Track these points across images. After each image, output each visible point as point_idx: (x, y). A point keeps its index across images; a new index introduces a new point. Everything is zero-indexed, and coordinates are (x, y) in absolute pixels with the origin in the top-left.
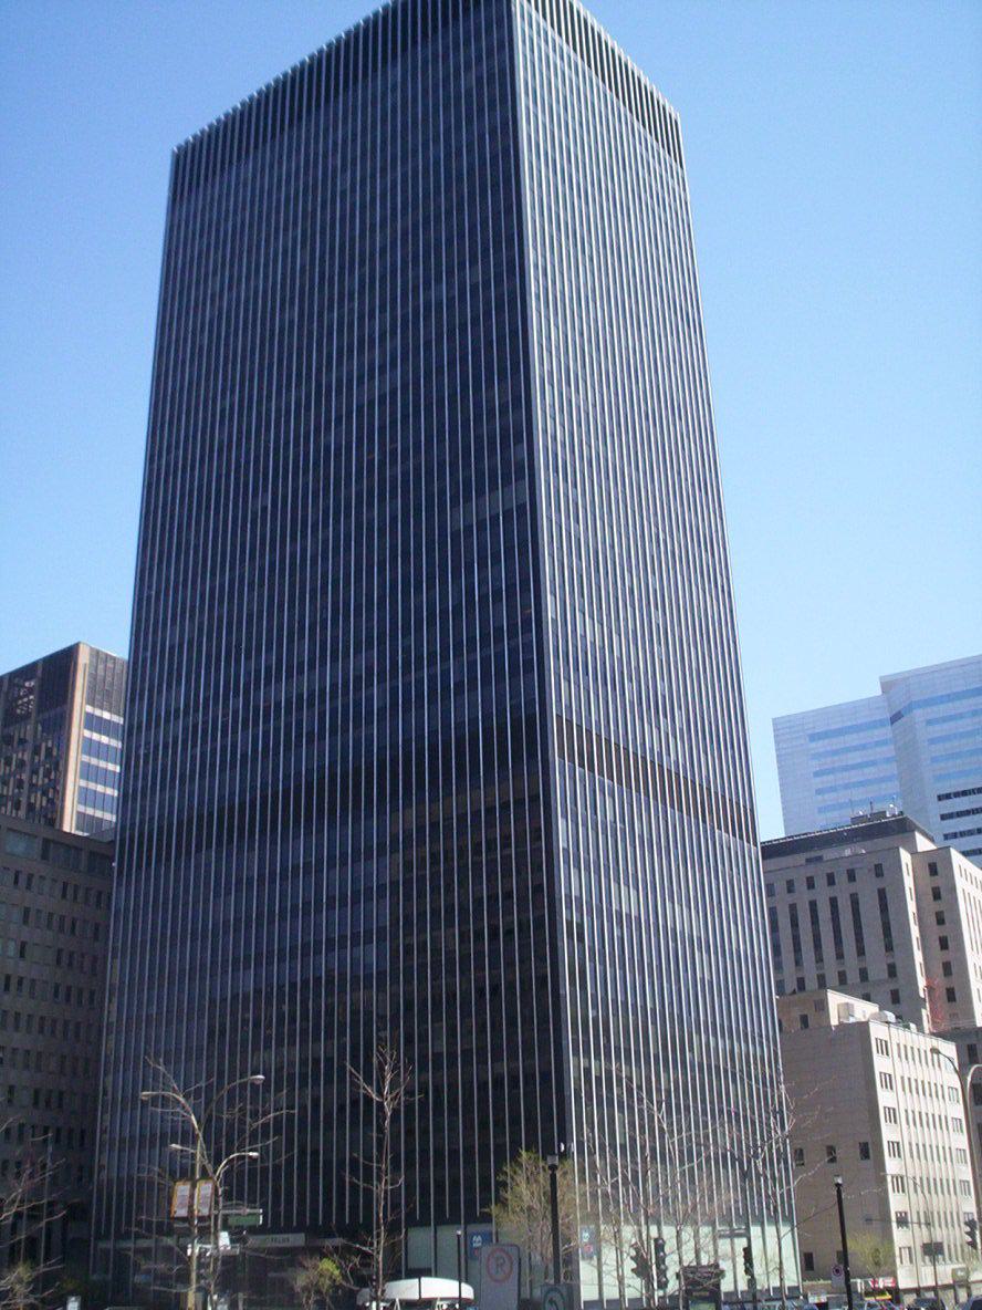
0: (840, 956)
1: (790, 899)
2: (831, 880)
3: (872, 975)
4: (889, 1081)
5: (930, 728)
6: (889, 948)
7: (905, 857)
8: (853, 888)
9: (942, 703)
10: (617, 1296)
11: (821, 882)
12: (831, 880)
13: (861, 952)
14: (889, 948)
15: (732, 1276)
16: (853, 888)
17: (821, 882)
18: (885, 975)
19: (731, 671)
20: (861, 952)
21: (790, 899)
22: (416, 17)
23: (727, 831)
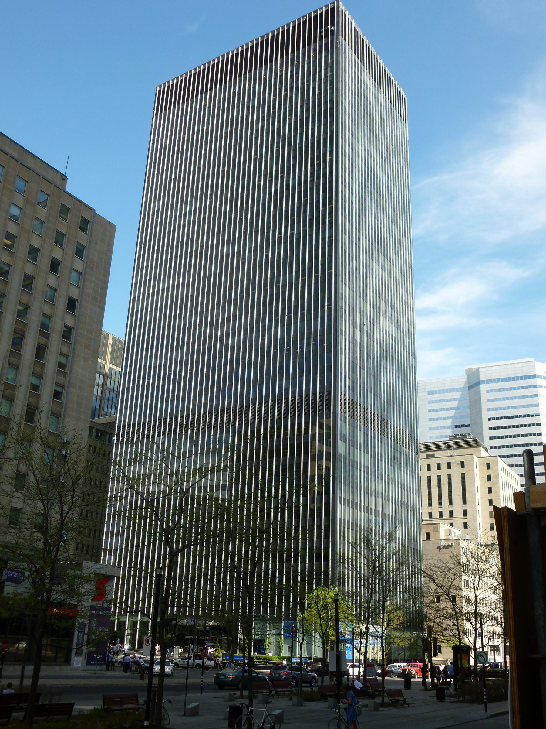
0: (440, 504)
1: (428, 473)
2: (439, 467)
3: (455, 515)
4: (494, 589)
5: (489, 413)
6: (464, 502)
7: (476, 459)
8: (449, 472)
9: (447, 390)
10: (42, 667)
11: (434, 467)
12: (439, 467)
13: (451, 503)
14: (464, 502)
15: (448, 725)
16: (449, 472)
17: (434, 467)
18: (462, 515)
19: (405, 389)
20: (451, 503)
21: (428, 473)
22: (205, 217)
23: (406, 448)
